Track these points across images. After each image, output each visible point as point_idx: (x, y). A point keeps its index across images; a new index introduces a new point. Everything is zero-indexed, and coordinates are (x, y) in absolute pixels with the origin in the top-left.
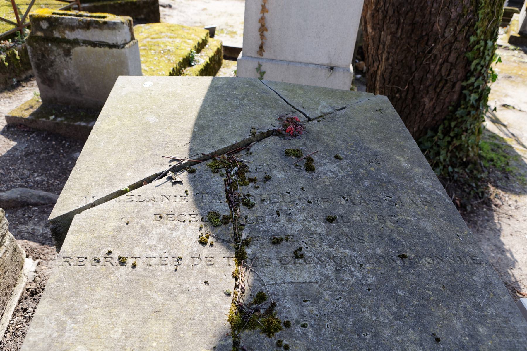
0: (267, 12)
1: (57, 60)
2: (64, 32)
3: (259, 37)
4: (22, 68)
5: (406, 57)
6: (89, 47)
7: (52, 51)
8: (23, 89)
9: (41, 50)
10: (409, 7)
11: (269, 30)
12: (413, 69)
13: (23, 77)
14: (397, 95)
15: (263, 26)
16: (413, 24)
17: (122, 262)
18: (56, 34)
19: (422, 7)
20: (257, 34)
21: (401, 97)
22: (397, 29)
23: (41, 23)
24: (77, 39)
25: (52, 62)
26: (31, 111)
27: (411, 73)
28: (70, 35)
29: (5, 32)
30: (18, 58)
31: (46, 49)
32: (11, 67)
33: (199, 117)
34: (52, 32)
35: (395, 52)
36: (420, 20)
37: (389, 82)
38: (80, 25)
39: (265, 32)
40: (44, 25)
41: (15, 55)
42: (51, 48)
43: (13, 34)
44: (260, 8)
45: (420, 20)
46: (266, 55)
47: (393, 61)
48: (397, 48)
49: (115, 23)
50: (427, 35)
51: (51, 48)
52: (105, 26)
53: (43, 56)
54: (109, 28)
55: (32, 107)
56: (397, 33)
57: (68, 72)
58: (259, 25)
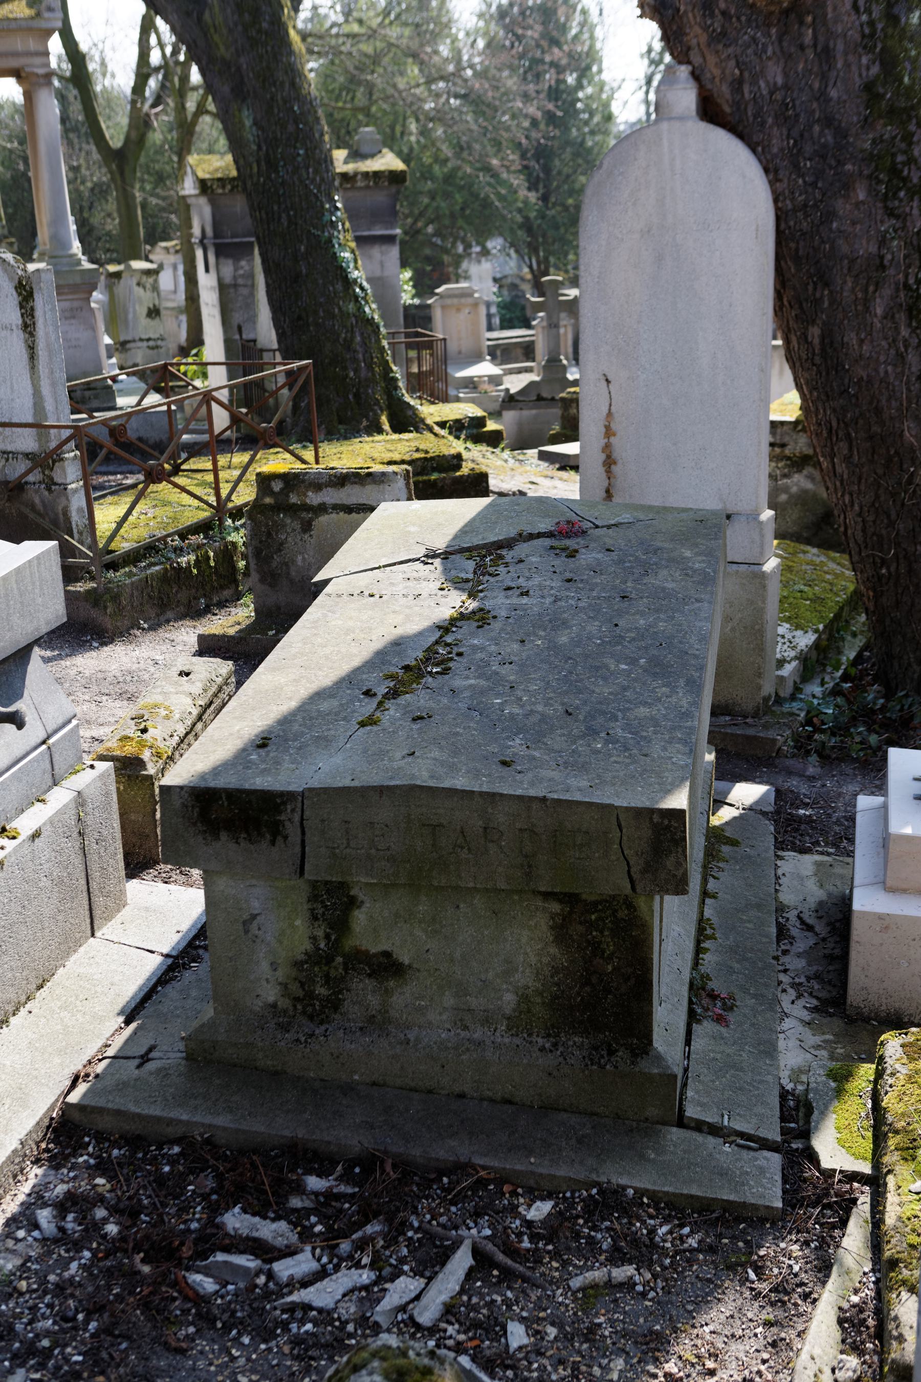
0: (614, 435)
1: (289, 539)
2: (305, 495)
3: (604, 475)
4: (215, 584)
5: (877, 497)
6: (341, 514)
7: (284, 526)
8: (214, 618)
9: (267, 525)
10: (857, 411)
11: (620, 462)
12: (893, 516)
13: (215, 599)
14: (884, 571)
15: (609, 457)
16: (871, 438)
17: (372, 596)
18: (294, 499)
19: (876, 408)
20: (601, 470)
21: (890, 573)
22: (850, 449)
23: (273, 484)
24: (324, 504)
25: (282, 544)
26: (237, 628)
27: (891, 524)
28: (314, 499)
29: (195, 520)
30: (212, 564)
31: (275, 522)
32: (200, 579)
33: (466, 525)
34: (288, 496)
35: (859, 490)
36: (879, 430)
37: (866, 547)
38: (331, 480)
39: (613, 467)
40: (277, 486)
41: (209, 558)
42: (282, 520)
43: (205, 524)
44: (604, 430)
45: (879, 430)
46: (616, 499)
47: (861, 508)
48: (859, 482)
49: (383, 474)
50: (897, 453)
51: (282, 520)
52: (369, 480)
53: (269, 534)
54: (375, 482)
55: (239, 624)
56: (851, 456)
57: (304, 558)
58: (603, 457)
